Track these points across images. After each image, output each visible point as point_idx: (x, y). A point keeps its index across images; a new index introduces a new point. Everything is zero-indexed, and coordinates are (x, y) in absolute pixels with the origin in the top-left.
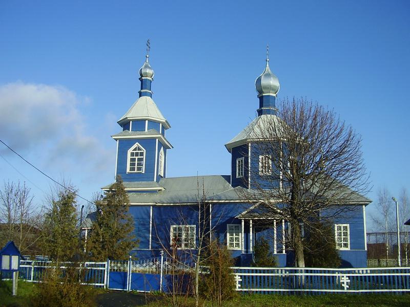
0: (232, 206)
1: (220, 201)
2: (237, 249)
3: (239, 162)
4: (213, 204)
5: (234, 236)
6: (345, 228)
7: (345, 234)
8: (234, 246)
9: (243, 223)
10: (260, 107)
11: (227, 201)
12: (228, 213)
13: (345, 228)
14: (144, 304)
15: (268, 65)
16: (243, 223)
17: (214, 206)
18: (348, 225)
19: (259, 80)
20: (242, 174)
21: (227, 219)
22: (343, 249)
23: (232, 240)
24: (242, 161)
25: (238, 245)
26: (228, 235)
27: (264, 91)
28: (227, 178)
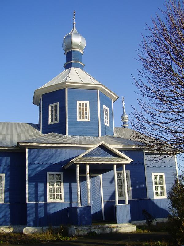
0: (53, 151)
1: (41, 145)
2: (59, 201)
3: (52, 108)
4: (31, 148)
5: (55, 186)
6: (161, 177)
7: (161, 183)
8: (56, 198)
9: (78, 169)
10: (67, 61)
11: (48, 145)
12: (49, 159)
13: (161, 177)
14: (183, 198)
15: (75, 27)
16: (78, 169)
17: (32, 151)
18: (163, 174)
19: (69, 37)
20: (56, 120)
21: (47, 166)
22: (160, 197)
23: (52, 190)
24: (56, 107)
25: (60, 196)
26: (48, 184)
27: (73, 47)
28: (37, 126)
